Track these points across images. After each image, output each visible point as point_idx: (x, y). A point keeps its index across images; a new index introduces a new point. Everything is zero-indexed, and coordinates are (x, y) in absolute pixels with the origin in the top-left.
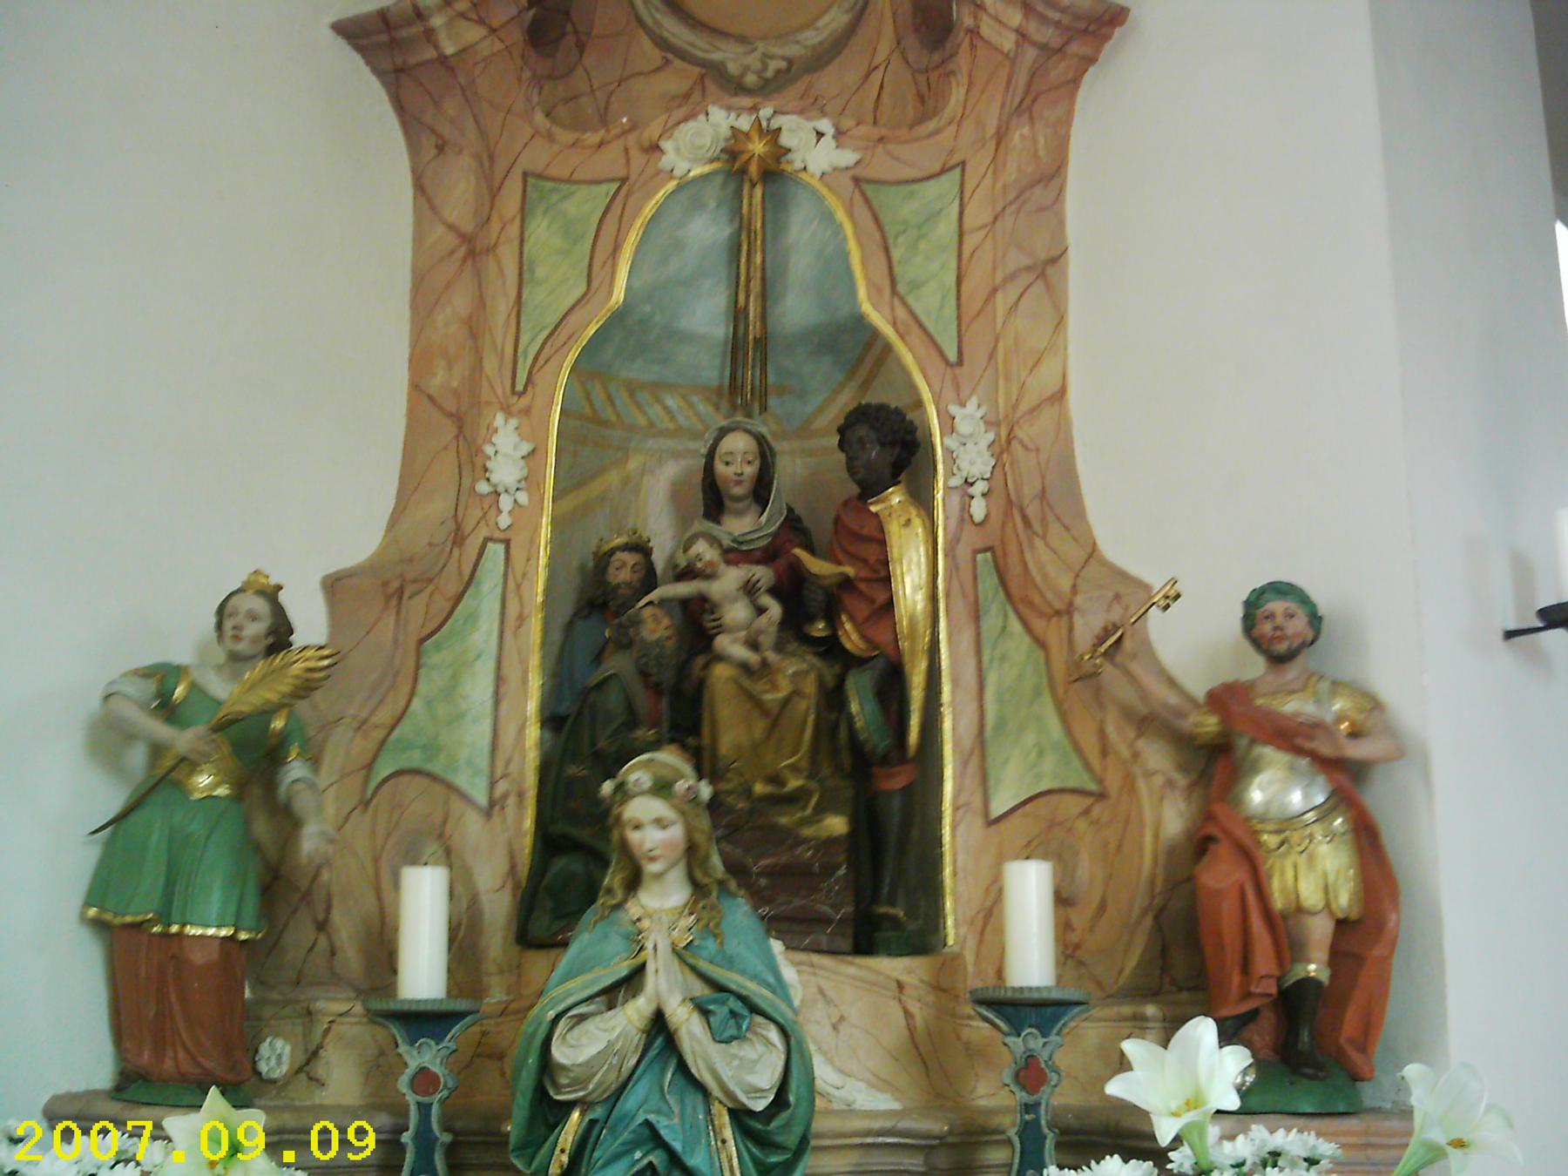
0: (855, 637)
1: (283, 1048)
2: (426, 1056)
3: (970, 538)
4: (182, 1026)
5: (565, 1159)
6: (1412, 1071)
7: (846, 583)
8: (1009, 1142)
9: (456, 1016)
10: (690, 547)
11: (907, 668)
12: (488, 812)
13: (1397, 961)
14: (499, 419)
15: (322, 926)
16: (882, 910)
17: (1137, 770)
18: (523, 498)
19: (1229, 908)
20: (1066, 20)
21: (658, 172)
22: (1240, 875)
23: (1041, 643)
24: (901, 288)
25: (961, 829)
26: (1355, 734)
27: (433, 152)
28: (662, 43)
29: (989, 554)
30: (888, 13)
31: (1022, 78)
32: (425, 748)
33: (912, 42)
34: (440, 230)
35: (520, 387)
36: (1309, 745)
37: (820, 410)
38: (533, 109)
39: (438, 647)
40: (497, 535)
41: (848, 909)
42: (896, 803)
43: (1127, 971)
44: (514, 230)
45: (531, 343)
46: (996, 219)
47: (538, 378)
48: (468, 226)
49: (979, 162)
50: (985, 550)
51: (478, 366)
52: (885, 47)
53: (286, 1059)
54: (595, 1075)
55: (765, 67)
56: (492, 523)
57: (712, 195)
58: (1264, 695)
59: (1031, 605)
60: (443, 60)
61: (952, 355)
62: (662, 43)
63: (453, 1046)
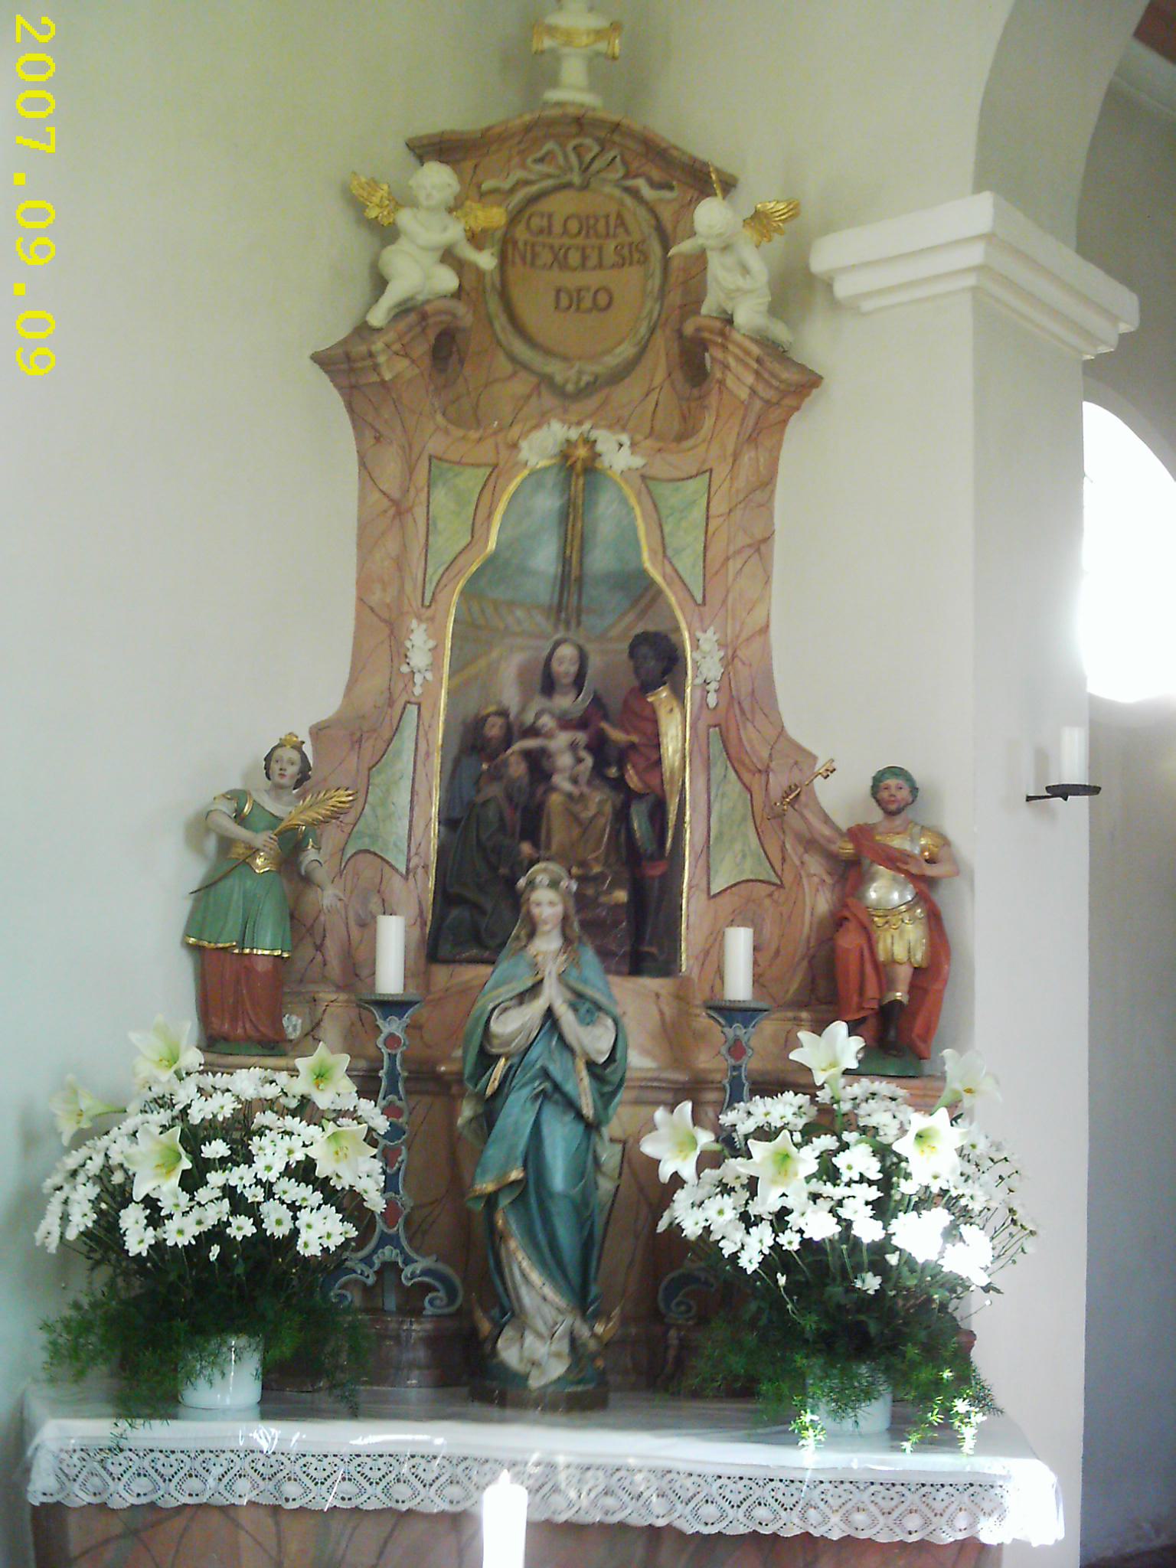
0: (635, 779)
1: (297, 1021)
2: (393, 1026)
3: (706, 718)
4: (248, 1005)
5: (496, 1083)
6: (947, 1053)
7: (632, 746)
8: (724, 1089)
9: (409, 1004)
10: (539, 718)
11: (668, 800)
12: (406, 878)
13: (947, 994)
14: (414, 624)
15: (319, 948)
16: (646, 949)
17: (803, 873)
18: (429, 676)
19: (853, 959)
20: (782, 387)
21: (516, 464)
22: (863, 941)
23: (749, 789)
24: (670, 553)
25: (693, 901)
26: (931, 861)
27: (372, 441)
28: (512, 358)
29: (717, 729)
30: (663, 353)
31: (750, 422)
32: (371, 836)
33: (678, 375)
34: (377, 495)
35: (427, 603)
36: (905, 867)
37: (613, 626)
38: (435, 412)
39: (379, 772)
40: (413, 699)
41: (627, 948)
42: (656, 884)
43: (791, 991)
44: (423, 496)
45: (434, 574)
46: (730, 511)
47: (440, 597)
48: (396, 494)
49: (721, 472)
50: (715, 726)
51: (401, 590)
52: (660, 376)
53: (299, 1027)
54: (514, 1040)
55: (579, 379)
56: (409, 691)
57: (550, 479)
58: (881, 834)
59: (743, 764)
60: (383, 383)
61: (699, 599)
62: (512, 358)
63: (408, 1021)
